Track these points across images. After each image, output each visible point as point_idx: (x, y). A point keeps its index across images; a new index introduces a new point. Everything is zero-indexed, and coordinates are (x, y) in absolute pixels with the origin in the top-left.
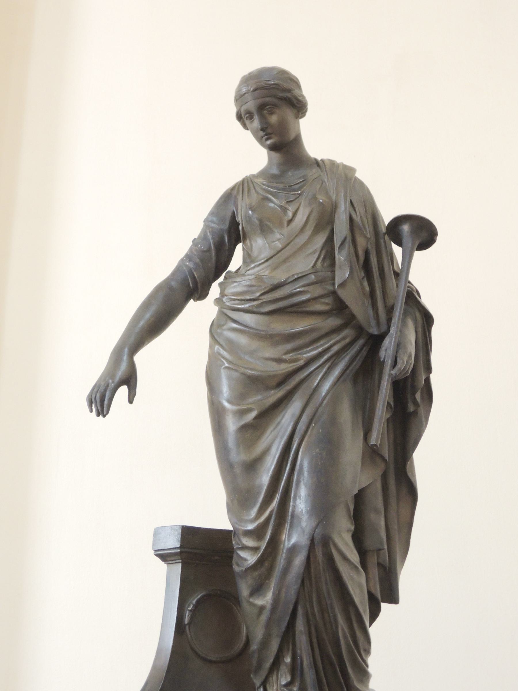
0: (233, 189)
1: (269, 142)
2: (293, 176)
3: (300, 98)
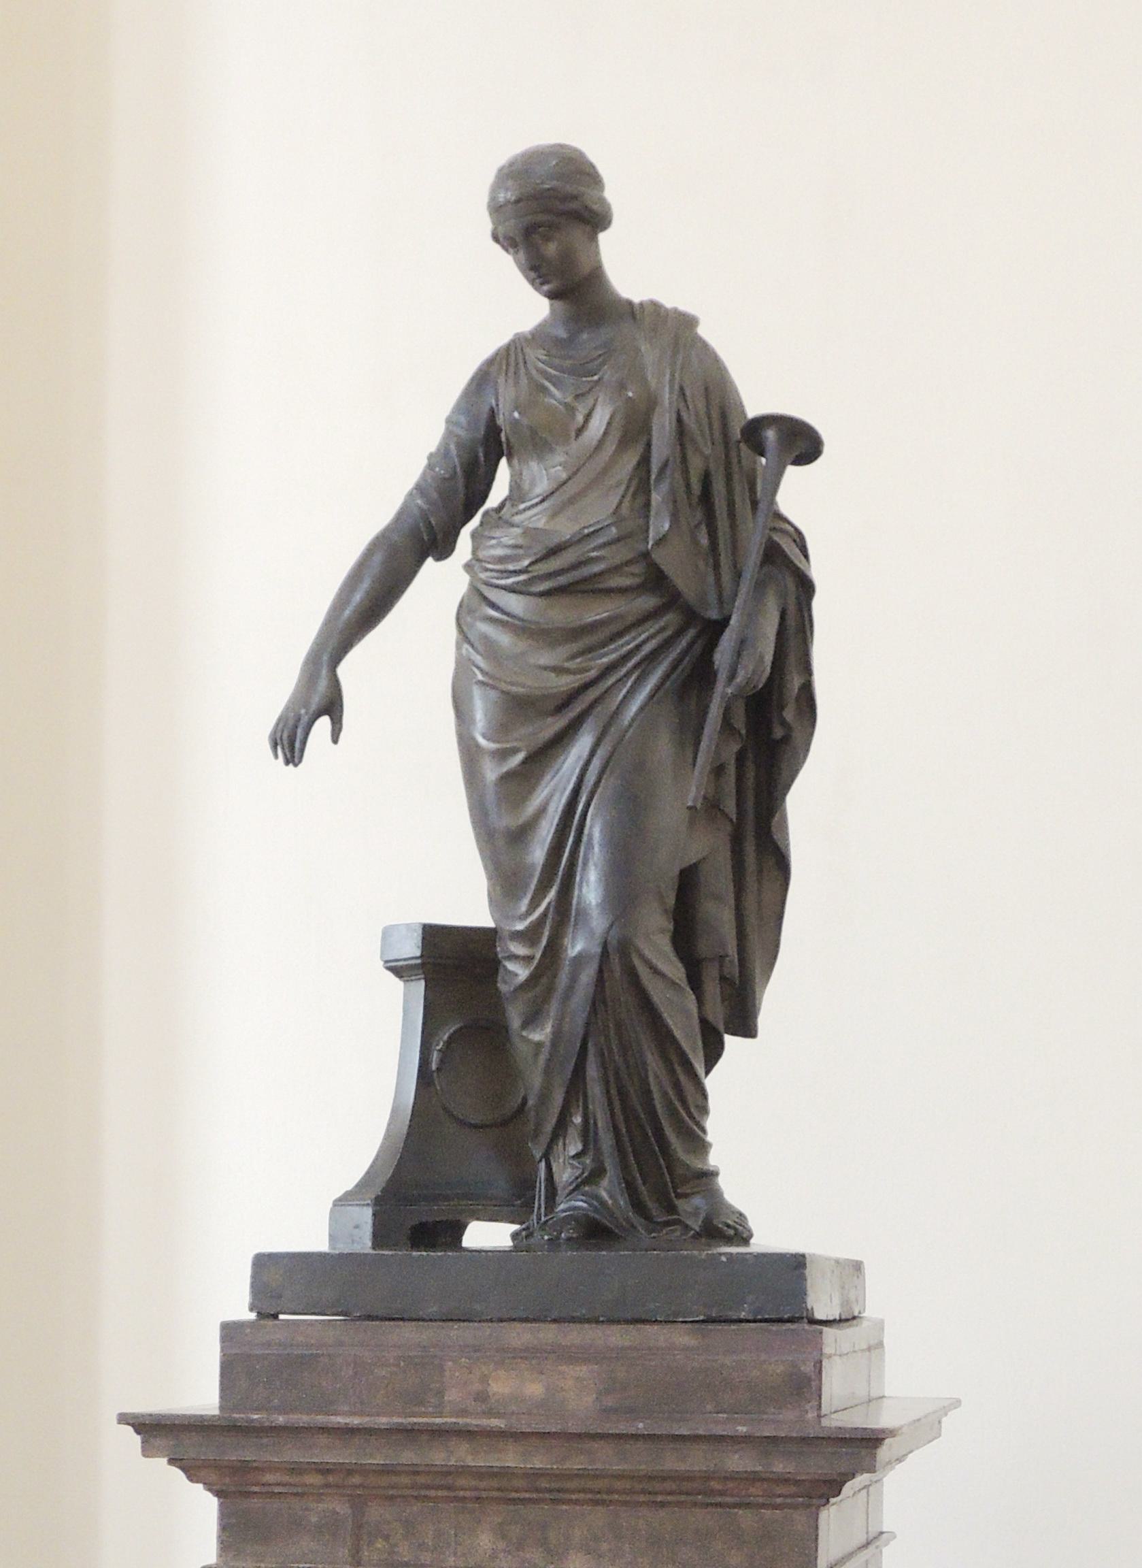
0: (490, 362)
1: (546, 288)
3: (595, 207)
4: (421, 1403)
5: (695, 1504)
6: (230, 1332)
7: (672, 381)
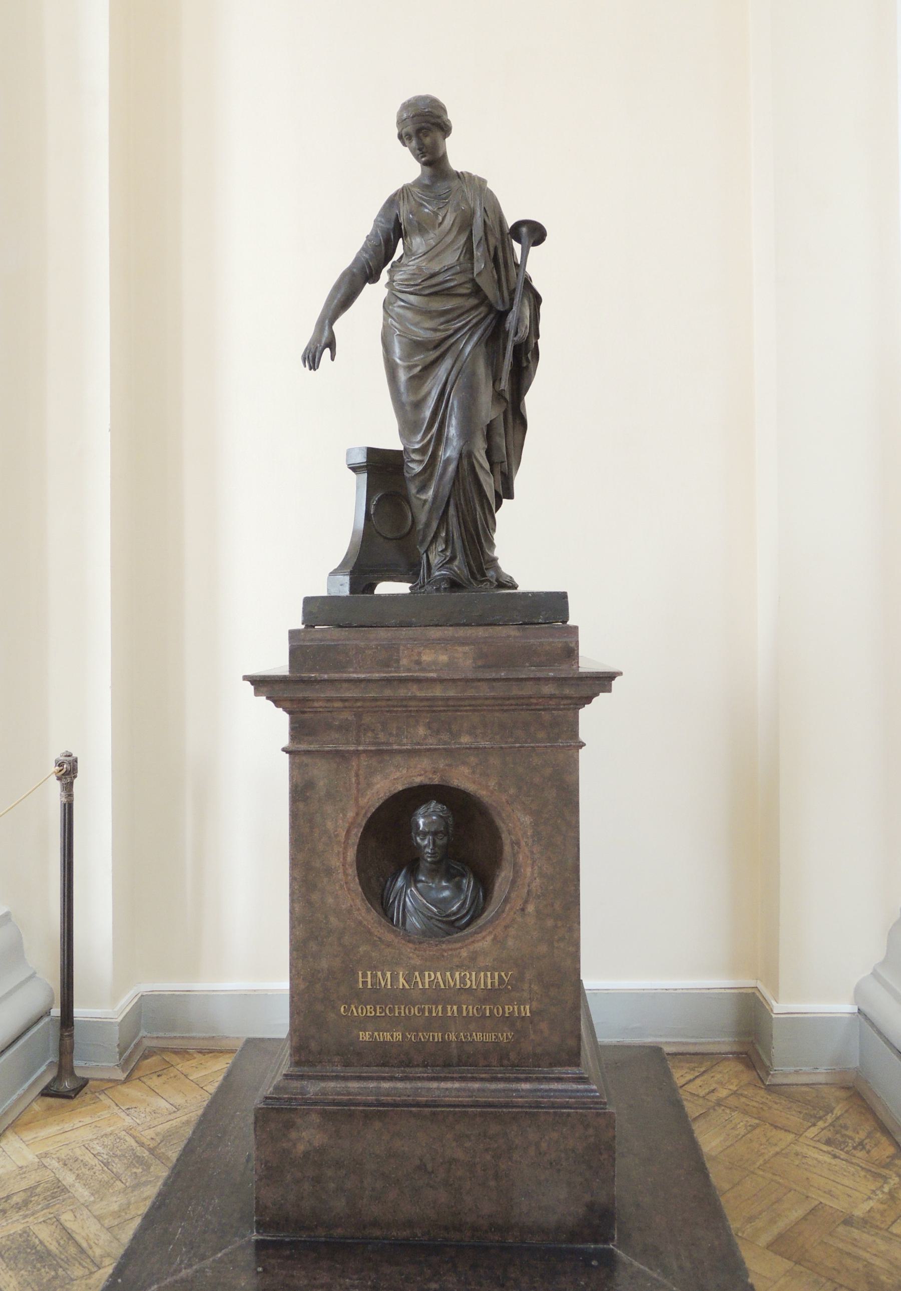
0: (395, 194)
2: (441, 187)
4: (388, 666)
5: (522, 710)
6: (293, 634)
7: (480, 204)
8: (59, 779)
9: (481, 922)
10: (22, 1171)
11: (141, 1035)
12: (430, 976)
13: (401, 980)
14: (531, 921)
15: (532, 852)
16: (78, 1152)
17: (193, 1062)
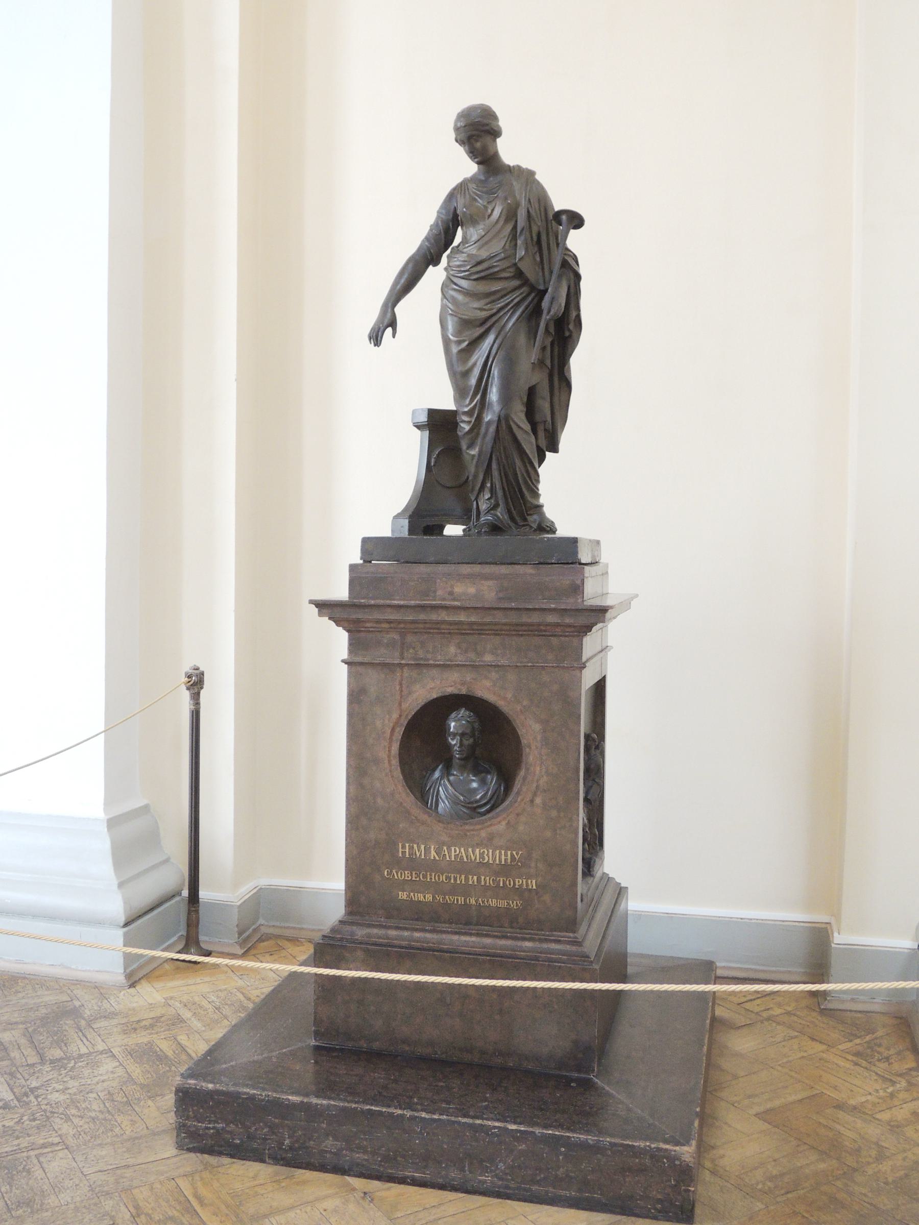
0: (454, 189)
6: (353, 568)
8: (188, 689)
9: (498, 810)
10: (152, 1007)
11: (259, 923)
12: (455, 851)
13: (433, 853)
14: (538, 811)
15: (541, 754)
16: (197, 999)
17: (301, 948)
